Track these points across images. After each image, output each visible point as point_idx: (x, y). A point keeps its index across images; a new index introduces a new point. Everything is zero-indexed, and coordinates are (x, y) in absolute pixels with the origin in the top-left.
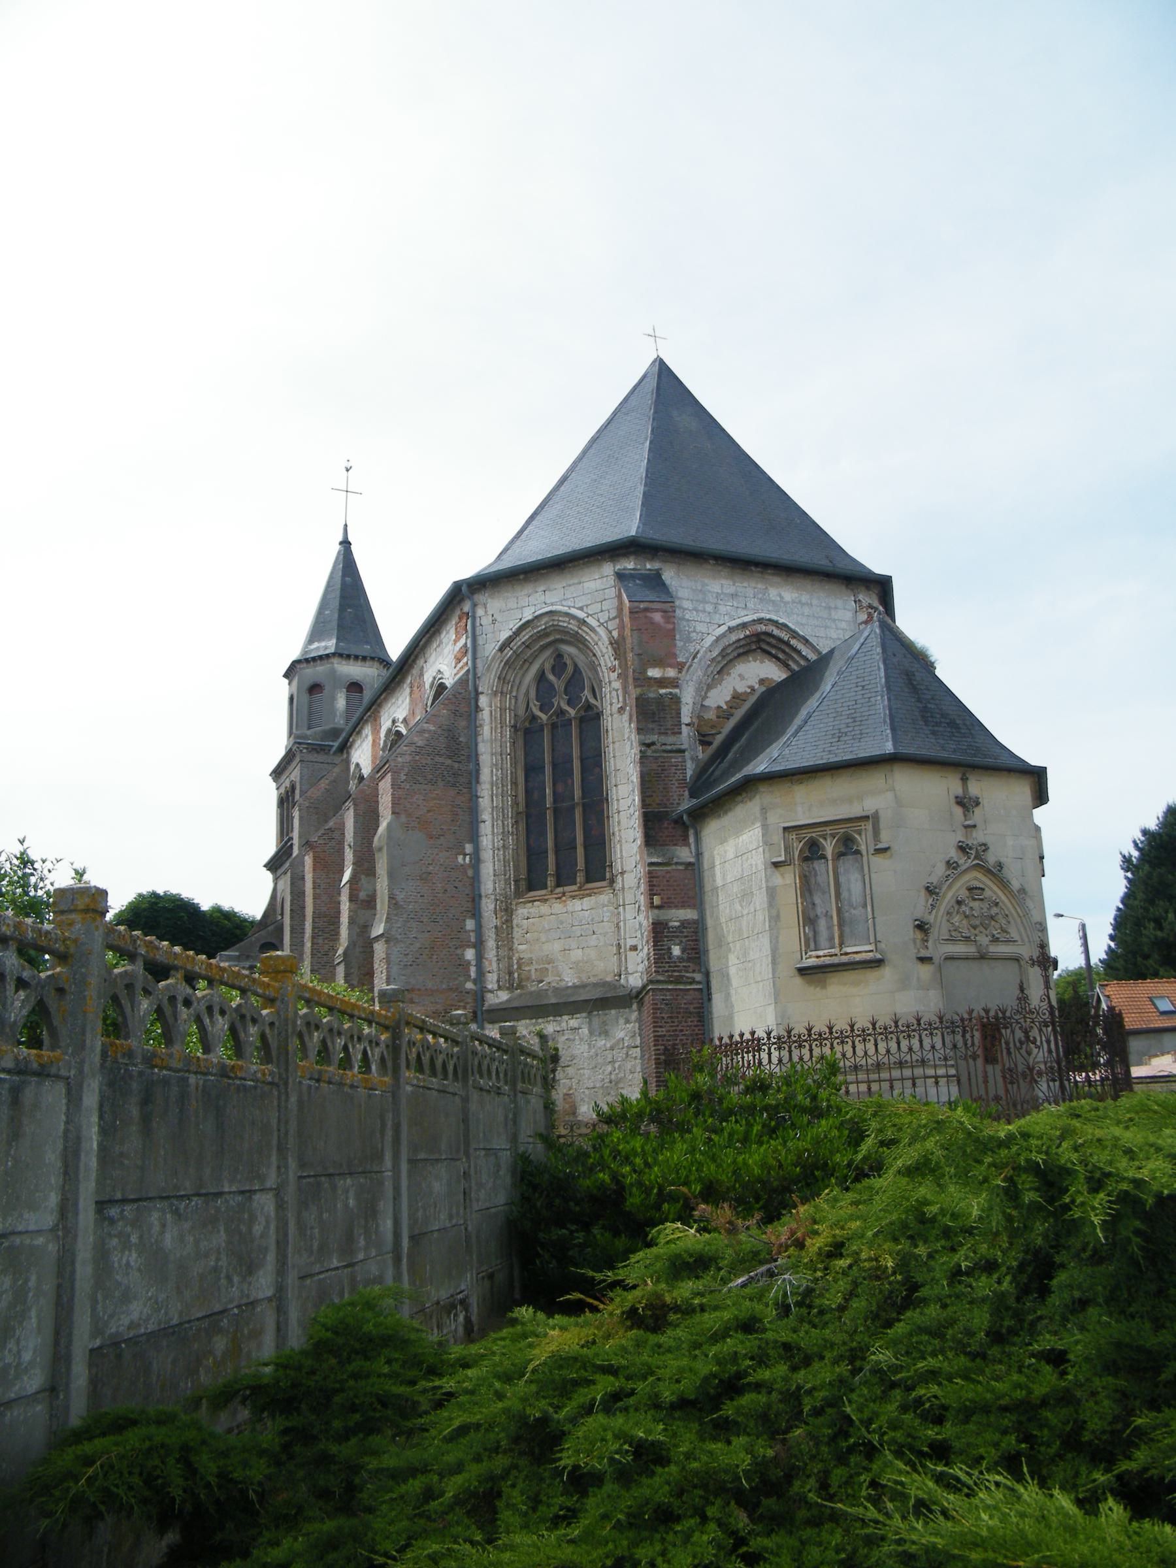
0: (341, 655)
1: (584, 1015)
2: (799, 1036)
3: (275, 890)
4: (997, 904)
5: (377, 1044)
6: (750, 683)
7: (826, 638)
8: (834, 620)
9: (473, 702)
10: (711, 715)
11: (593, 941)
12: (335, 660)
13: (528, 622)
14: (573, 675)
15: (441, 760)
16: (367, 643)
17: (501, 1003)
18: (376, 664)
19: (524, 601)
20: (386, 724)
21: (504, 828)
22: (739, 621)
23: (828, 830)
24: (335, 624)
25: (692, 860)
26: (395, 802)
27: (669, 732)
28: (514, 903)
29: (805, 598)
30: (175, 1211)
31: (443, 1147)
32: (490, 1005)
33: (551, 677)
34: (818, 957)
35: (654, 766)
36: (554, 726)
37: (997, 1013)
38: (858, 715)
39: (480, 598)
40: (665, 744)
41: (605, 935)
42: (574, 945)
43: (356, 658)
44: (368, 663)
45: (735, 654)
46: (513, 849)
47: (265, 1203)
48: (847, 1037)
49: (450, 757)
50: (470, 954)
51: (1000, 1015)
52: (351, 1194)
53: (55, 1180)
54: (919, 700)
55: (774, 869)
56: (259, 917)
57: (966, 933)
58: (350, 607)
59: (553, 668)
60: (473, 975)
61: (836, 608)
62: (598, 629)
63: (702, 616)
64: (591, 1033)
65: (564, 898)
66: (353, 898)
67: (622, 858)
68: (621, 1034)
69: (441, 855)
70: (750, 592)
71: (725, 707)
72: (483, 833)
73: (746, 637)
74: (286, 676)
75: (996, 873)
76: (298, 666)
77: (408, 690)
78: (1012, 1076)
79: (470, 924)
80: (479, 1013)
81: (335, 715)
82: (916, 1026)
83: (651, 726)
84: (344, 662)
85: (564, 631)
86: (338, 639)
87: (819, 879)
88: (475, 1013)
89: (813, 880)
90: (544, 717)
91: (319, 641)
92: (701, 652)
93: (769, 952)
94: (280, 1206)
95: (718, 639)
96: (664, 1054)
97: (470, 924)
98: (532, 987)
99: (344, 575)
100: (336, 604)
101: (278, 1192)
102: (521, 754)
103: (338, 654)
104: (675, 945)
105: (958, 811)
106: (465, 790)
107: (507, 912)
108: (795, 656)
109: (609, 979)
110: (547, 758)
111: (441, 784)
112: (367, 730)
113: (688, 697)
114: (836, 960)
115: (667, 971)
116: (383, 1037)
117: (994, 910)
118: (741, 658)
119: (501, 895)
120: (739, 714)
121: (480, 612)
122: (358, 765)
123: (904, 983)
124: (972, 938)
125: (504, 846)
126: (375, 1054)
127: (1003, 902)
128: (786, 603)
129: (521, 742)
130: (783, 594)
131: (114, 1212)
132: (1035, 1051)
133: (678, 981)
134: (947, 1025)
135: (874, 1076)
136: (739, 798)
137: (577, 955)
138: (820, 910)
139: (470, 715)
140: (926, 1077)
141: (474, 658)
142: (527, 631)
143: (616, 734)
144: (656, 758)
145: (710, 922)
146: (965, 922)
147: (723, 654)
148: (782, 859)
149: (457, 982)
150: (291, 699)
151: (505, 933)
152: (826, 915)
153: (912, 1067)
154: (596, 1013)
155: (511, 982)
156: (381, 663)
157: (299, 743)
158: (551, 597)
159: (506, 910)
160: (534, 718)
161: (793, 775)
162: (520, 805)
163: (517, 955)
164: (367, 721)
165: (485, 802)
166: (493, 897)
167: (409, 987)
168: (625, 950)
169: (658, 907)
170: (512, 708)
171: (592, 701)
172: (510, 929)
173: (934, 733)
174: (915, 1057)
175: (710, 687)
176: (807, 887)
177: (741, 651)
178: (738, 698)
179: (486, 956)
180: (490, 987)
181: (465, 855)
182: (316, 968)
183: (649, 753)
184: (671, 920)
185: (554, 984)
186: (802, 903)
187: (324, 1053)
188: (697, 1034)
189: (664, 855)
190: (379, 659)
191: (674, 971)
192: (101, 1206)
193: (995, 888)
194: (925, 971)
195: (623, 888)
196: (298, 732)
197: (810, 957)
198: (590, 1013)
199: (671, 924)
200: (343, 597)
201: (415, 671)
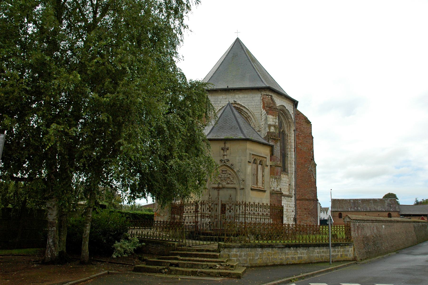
8: (254, 100)
29: (246, 96)
51: (202, 202)
75: (231, 167)
105: (222, 151)
117: (229, 176)
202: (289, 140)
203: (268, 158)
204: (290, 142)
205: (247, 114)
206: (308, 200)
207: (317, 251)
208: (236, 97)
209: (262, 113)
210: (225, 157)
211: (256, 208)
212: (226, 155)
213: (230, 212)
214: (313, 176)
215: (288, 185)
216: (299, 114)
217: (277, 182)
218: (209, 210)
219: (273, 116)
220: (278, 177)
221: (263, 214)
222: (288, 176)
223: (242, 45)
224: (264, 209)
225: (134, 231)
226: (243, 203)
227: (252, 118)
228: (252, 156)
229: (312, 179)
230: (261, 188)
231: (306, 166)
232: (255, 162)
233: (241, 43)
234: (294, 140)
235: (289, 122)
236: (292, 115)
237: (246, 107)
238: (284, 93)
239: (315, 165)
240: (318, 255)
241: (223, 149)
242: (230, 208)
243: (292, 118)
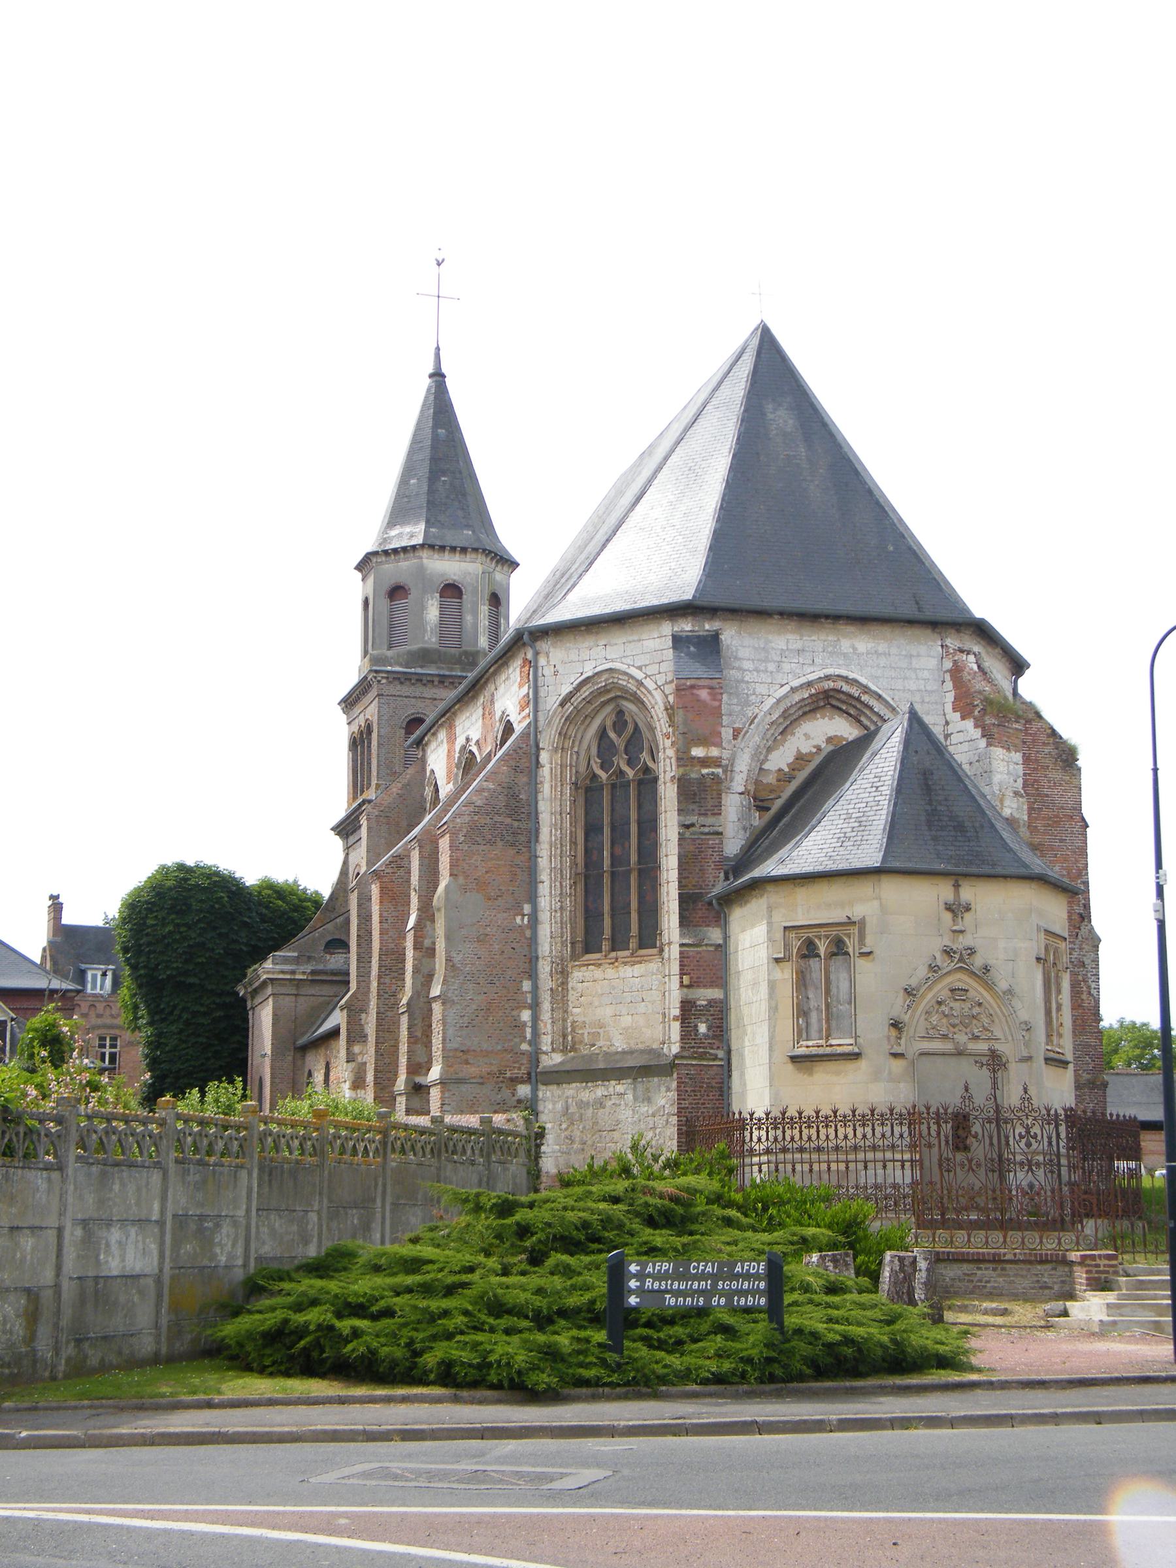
0: (432, 547)
1: (629, 1081)
2: (809, 1117)
3: (345, 863)
4: (980, 1004)
5: (374, 1142)
6: (815, 743)
7: (904, 690)
9: (533, 758)
10: (771, 779)
11: (642, 1008)
12: (425, 554)
13: (588, 678)
14: (634, 733)
15: (499, 819)
16: (468, 526)
17: (554, 1065)
18: (481, 558)
19: (585, 655)
20: (460, 741)
21: (561, 890)
22: (803, 680)
23: (823, 932)
24: (423, 500)
25: (721, 942)
26: (452, 866)
27: (709, 813)
28: (570, 966)
29: (882, 647)
30: (279, 1215)
31: (419, 1197)
32: (544, 1067)
33: (612, 735)
34: (807, 1047)
35: (692, 848)
36: (614, 786)
37: (938, 1109)
38: (864, 819)
39: (543, 645)
40: (704, 826)
41: (653, 1002)
42: (624, 1012)
43: (453, 549)
44: (469, 556)
45: (800, 713)
46: (570, 911)
47: (313, 1217)
48: (813, 1122)
49: (510, 816)
50: (526, 1015)
51: (941, 1111)
52: (356, 1217)
53: (245, 1200)
54: (930, 803)
55: (775, 964)
56: (326, 893)
57: (944, 1031)
58: (444, 473)
59: (614, 724)
60: (529, 1036)
61: (918, 656)
62: (654, 692)
63: (764, 677)
64: (635, 1099)
65: (616, 964)
66: (417, 946)
67: (669, 929)
68: (663, 1102)
69: (499, 916)
70: (819, 645)
71: (787, 770)
72: (541, 894)
73: (811, 696)
74: (360, 567)
75: (984, 975)
76: (374, 560)
77: (480, 711)
78: (948, 1165)
79: (527, 985)
80: (533, 1074)
81: (425, 631)
82: (890, 1116)
83: (692, 807)
84: (436, 556)
85: (623, 689)
86: (427, 522)
87: (814, 975)
88: (529, 1074)
89: (808, 977)
90: (603, 775)
91: (403, 523)
92: (759, 717)
93: (767, 1040)
94: (320, 1219)
95: (779, 701)
96: (686, 1125)
97: (527, 985)
98: (585, 1051)
99: (436, 426)
100: (424, 470)
101: (319, 1212)
102: (581, 812)
103: (428, 546)
104: (702, 1022)
105: (948, 916)
106: (524, 850)
107: (563, 974)
108: (868, 712)
109: (655, 1046)
110: (606, 820)
111: (500, 844)
112: (442, 735)
113: (743, 766)
114: (821, 1051)
115: (693, 1047)
116: (377, 1138)
117: (976, 1010)
118: (809, 716)
119: (557, 957)
120: (802, 776)
121: (542, 661)
122: (432, 771)
123: (876, 1076)
124: (950, 1036)
125: (561, 908)
126: (372, 1148)
128: (859, 655)
129: (581, 801)
131: (260, 1213)
132: (975, 1144)
133: (702, 1056)
134: (912, 1118)
135: (851, 1157)
136: (754, 893)
137: (627, 1021)
138: (813, 1004)
139: (530, 771)
140: (894, 1161)
141: (536, 711)
142: (588, 686)
143: (668, 804)
144: (694, 840)
145: (733, 1003)
146: (944, 1021)
147: (785, 715)
148: (782, 955)
149: (513, 1043)
150: (366, 602)
151: (561, 995)
152: (817, 1009)
153: (884, 1151)
154: (640, 1080)
155: (566, 1044)
156: (487, 555)
157: (376, 672)
158: (614, 652)
159: (562, 972)
160: (594, 776)
161: (795, 879)
162: (579, 865)
163: (571, 1018)
164: (442, 725)
165: (543, 863)
166: (549, 959)
167: (464, 1048)
168: (669, 1018)
169: (688, 987)
170: (574, 764)
171: (650, 764)
172: (565, 991)
173: (935, 839)
174: (868, 1143)
175: (769, 750)
176: (802, 982)
177: (807, 709)
178: (802, 759)
179: (542, 1018)
180: (544, 1049)
181: (523, 915)
182: (382, 1010)
183: (687, 835)
184: (699, 999)
185: (605, 1049)
186: (797, 997)
187: (343, 1151)
188: (718, 1108)
189: (695, 936)
190: (484, 550)
191: (700, 1047)
192: (258, 1210)
193: (981, 990)
194: (898, 1065)
195: (669, 959)
196: (375, 652)
197: (801, 1047)
198: (635, 1079)
199: (698, 1003)
200: (434, 459)
201: (487, 693)
214: (1089, 987)
218: (1024, 1141)
225: (30, 1244)
229: (1084, 996)
237: (884, 695)
238: (432, 398)
241: (949, 908)
242: (1028, 1132)
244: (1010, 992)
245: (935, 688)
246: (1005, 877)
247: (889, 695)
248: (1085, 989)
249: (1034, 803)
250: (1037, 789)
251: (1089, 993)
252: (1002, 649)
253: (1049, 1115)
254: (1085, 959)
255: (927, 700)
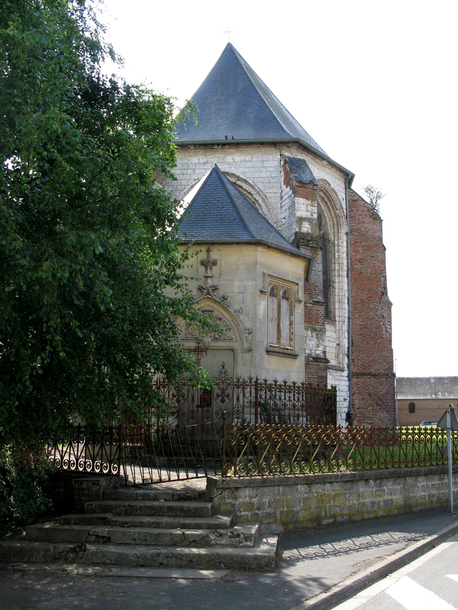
4: (220, 319)
29: (248, 158)
105: (202, 269)
127: (226, 318)
130: (235, 158)
202: (337, 254)
203: (301, 284)
204: (339, 258)
205: (252, 195)
206: (375, 376)
207: (423, 486)
208: (228, 161)
209: (283, 194)
210: (209, 280)
211: (280, 391)
212: (211, 277)
213: (223, 401)
215: (334, 345)
216: (356, 201)
217: (317, 337)
218: (175, 399)
219: (307, 199)
220: (318, 327)
221: (294, 405)
222: (335, 326)
223: (238, 57)
224: (296, 395)
226: (251, 382)
227: (263, 204)
228: (268, 280)
229: (384, 333)
230: (288, 349)
231: (371, 306)
232: (273, 294)
233: (237, 54)
234: (347, 255)
235: (337, 216)
236: (342, 201)
237: (248, 180)
239: (389, 305)
240: (423, 494)
241: (202, 263)
242: (223, 392)
243: (342, 208)
244: (239, 311)
245: (276, 175)
246: (238, 243)
247: (251, 181)
248: (384, 329)
249: (357, 239)
250: (359, 233)
251: (387, 331)
252: (328, 162)
253: (238, 382)
254: (384, 314)
255: (272, 181)
